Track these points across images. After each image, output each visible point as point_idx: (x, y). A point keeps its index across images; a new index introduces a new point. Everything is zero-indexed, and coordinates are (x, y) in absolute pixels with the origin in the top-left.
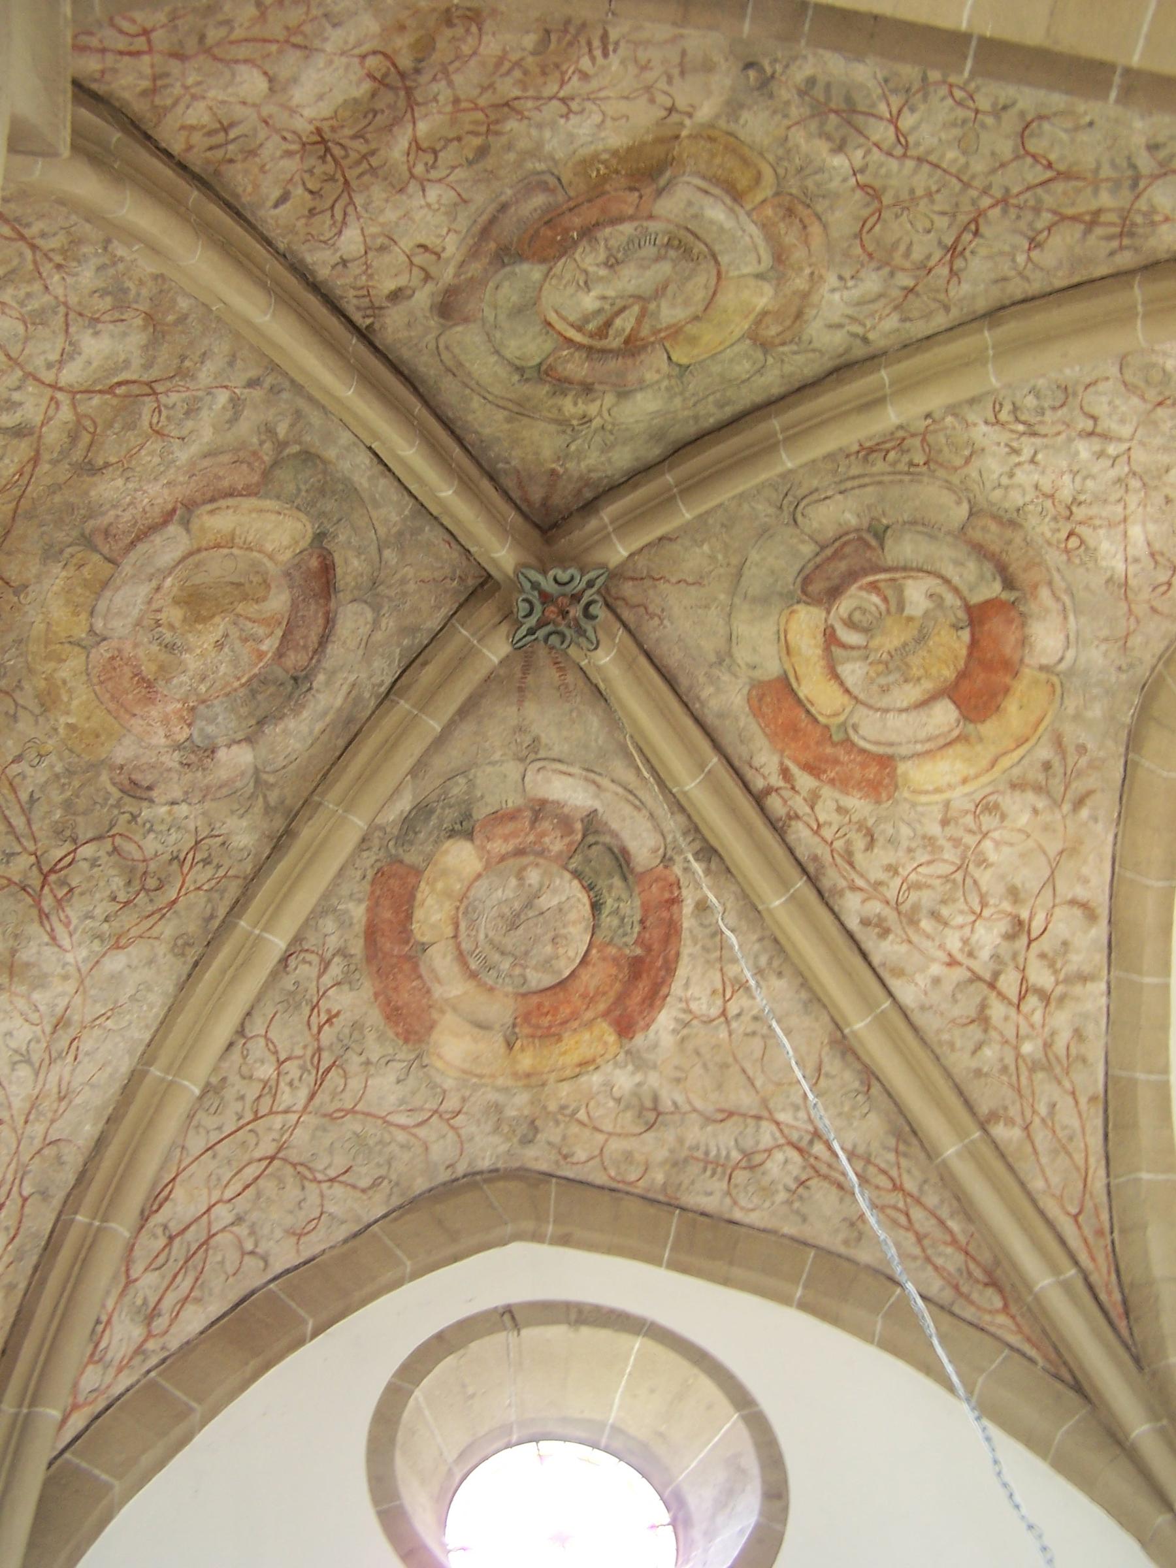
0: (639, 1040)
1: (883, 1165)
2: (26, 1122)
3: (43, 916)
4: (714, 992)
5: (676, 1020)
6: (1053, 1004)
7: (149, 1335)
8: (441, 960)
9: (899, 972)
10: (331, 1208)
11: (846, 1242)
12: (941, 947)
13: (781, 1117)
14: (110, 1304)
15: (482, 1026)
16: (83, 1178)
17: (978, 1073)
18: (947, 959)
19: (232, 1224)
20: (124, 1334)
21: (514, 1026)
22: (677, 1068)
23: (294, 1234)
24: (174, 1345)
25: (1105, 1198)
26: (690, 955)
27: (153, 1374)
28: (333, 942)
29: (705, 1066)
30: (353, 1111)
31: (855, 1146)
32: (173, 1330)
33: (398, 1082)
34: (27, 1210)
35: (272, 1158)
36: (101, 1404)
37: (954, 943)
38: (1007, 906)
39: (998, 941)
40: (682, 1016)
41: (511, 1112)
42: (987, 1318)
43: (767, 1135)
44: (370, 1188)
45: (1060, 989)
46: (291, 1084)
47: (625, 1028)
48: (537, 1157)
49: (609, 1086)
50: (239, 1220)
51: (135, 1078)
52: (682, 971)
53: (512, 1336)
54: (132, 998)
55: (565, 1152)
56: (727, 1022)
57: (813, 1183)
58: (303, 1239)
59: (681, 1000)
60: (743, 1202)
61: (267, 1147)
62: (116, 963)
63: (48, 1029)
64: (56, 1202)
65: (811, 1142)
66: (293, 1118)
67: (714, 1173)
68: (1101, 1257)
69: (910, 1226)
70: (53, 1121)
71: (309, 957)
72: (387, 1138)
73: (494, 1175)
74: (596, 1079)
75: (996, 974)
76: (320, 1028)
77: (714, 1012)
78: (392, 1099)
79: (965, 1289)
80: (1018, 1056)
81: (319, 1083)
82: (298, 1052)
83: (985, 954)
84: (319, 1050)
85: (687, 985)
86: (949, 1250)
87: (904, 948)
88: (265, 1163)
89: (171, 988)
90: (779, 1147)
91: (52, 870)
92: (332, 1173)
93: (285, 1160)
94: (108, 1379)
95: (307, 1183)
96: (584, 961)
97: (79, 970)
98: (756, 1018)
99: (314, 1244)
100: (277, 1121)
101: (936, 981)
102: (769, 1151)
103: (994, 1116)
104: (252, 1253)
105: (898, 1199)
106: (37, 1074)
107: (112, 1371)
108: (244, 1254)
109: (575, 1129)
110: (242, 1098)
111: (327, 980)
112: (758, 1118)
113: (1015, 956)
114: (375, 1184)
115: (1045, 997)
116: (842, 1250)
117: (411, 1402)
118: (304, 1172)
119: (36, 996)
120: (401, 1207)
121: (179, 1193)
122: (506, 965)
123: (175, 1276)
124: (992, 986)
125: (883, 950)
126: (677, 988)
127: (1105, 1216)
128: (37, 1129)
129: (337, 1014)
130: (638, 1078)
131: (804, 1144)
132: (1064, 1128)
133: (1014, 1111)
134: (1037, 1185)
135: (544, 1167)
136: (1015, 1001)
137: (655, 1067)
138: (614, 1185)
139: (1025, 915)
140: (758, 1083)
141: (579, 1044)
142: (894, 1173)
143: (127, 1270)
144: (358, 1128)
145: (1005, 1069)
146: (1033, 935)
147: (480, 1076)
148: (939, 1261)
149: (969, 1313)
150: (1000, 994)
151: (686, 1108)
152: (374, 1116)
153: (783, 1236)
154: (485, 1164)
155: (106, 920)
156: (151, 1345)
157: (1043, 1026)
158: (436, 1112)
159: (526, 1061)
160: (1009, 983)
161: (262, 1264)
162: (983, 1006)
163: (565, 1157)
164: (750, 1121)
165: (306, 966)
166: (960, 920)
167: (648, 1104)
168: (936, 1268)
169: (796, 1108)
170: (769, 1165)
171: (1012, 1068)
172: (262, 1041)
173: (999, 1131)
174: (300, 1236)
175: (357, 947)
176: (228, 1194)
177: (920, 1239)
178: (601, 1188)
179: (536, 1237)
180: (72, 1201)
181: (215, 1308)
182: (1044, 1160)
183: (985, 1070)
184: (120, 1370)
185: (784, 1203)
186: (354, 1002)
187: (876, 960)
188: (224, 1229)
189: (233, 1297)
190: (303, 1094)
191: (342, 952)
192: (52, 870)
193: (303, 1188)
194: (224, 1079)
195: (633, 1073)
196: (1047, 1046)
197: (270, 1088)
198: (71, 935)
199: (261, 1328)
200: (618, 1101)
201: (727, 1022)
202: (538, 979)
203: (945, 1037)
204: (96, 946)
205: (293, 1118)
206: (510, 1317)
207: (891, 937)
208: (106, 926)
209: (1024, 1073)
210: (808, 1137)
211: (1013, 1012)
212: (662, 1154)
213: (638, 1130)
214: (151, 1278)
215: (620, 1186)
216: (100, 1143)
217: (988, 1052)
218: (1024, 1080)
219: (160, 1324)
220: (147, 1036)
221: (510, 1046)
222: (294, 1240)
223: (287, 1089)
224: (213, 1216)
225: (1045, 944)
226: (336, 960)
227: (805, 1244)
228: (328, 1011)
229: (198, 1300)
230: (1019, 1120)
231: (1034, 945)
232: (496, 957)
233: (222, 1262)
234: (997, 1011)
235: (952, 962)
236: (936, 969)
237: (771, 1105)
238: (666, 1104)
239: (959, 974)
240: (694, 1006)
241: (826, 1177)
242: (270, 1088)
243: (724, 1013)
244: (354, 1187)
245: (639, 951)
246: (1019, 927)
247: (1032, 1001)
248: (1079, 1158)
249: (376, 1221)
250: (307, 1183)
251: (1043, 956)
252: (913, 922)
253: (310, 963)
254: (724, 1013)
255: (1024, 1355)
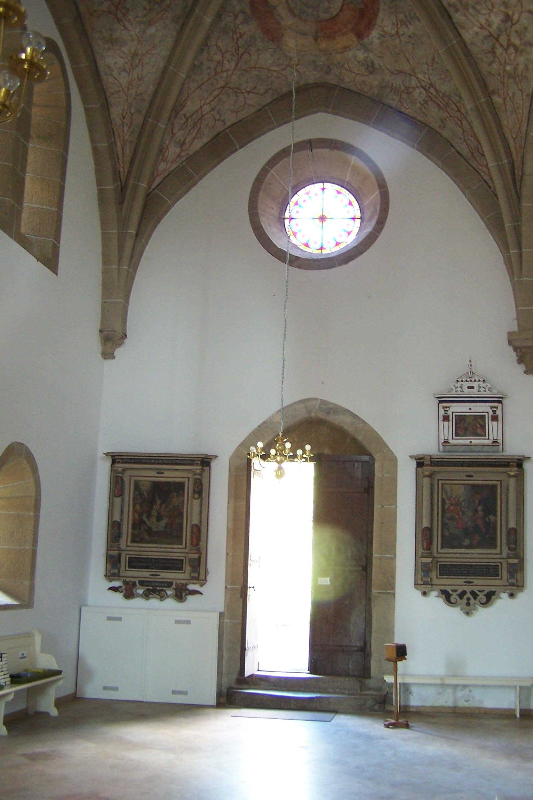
0: (366, 40)
1: (455, 101)
2: (128, 89)
3: (120, 21)
4: (393, 24)
5: (379, 34)
6: (519, 53)
7: (182, 150)
8: (282, 11)
9: (463, 28)
10: (249, 102)
11: (440, 127)
12: (478, 21)
13: (420, 76)
14: (167, 142)
15: (304, 34)
16: (151, 103)
17: (490, 74)
18: (480, 26)
19: (210, 111)
20: (173, 151)
21: (317, 32)
22: (381, 52)
23: (235, 112)
24: (191, 153)
25: (524, 135)
26: (383, 9)
27: (184, 163)
28: (238, 8)
29: (391, 53)
30: (255, 68)
31: (445, 92)
32: (191, 148)
33: (271, 56)
34: (133, 117)
35: (223, 88)
36: (167, 173)
37: (482, 20)
38: (503, 9)
39: (500, 22)
40: (381, 32)
41: (319, 63)
42: (480, 167)
43: (414, 82)
44: (265, 93)
45: (522, 47)
46: (228, 61)
47: (360, 36)
48: (331, 79)
49: (355, 57)
50: (213, 109)
51: (166, 68)
52: (381, 15)
53: (309, 152)
54: (161, 41)
55: (341, 78)
56: (399, 37)
57: (430, 103)
58: (239, 113)
59: (380, 27)
60: (405, 105)
61: (222, 83)
62: (152, 30)
63: (130, 58)
64: (144, 113)
65: (429, 87)
66: (230, 73)
67: (395, 93)
68: (519, 157)
69: (461, 127)
70: (138, 88)
71: (231, 14)
72: (270, 75)
73: (316, 85)
74: (350, 54)
75: (499, 36)
76: (238, 40)
77: (394, 32)
78: (270, 61)
79: (475, 155)
80: (505, 70)
81: (239, 59)
82: (230, 49)
83: (495, 26)
84: (238, 47)
85: (382, 21)
86: (473, 139)
87: (464, 18)
88: (221, 89)
89: (175, 34)
90: (418, 87)
91: (119, 4)
92: (248, 89)
93: (229, 87)
94: (168, 165)
95: (238, 94)
96: (341, 9)
97: (138, 37)
98: (410, 37)
99: (243, 114)
100: (225, 75)
101: (477, 33)
102: (414, 88)
103: (494, 92)
104: (219, 120)
105: (457, 114)
106: (129, 75)
107: (169, 163)
108: (215, 120)
109: (344, 71)
110: (210, 68)
111: (238, 22)
112: (410, 75)
113: (506, 29)
114: (267, 91)
115: (516, 48)
116: (438, 129)
117: (269, 174)
118: (237, 91)
119: (123, 49)
120: (277, 99)
121: (189, 103)
122: (310, 11)
123: (190, 131)
124: (497, 40)
125: (458, 17)
126: (379, 22)
127: (523, 142)
128: (133, 91)
129: (244, 34)
130: (366, 55)
131: (427, 88)
132: (517, 103)
133: (501, 92)
134: (504, 122)
135: (334, 82)
136: (505, 47)
137: (371, 52)
138: (359, 91)
139: (510, 13)
140: (411, 62)
141: (342, 41)
142: (458, 105)
143: (172, 131)
144: (257, 73)
145: (499, 75)
146: (514, 22)
147: (305, 51)
148: (469, 142)
149: (474, 164)
150: (500, 43)
151: (384, 68)
152: (263, 68)
153: (418, 120)
154: (311, 81)
155: (144, 16)
156: (182, 154)
157: (514, 61)
158: (288, 65)
159: (323, 45)
160: (503, 40)
161: (223, 123)
162: (494, 47)
163: (342, 80)
164: (407, 76)
165: (229, 18)
166: (484, 11)
167: (370, 64)
168: (467, 145)
169: (425, 73)
170: (414, 93)
171: (502, 75)
172: (215, 47)
173: (495, 98)
174: (237, 113)
175: (248, 10)
176: (208, 101)
177: (464, 132)
178: (355, 92)
179: (326, 111)
180: (148, 113)
181: (206, 140)
182: (508, 114)
183: (493, 73)
184: (172, 162)
185: (418, 108)
186: (250, 29)
187: (455, 21)
188: (207, 113)
189: (212, 135)
190: (233, 65)
191: (242, 11)
192: (119, 4)
193: (237, 96)
194: (202, 63)
195: (364, 53)
196: (515, 69)
197: (220, 63)
198: (132, 25)
199: (220, 147)
200: (359, 62)
201: (399, 37)
202: (324, 16)
203: (480, 56)
204: (142, 26)
205: (230, 73)
206: (310, 144)
207: (459, 13)
208: (145, 19)
209: (506, 78)
210: (428, 85)
211: (504, 52)
212: (376, 83)
213: (367, 74)
214: (181, 133)
215: (362, 93)
216: (156, 92)
217: (495, 66)
218: (506, 81)
219: (185, 147)
220: (169, 53)
221: (316, 40)
222: (235, 114)
223: (227, 63)
224: (203, 109)
225: (518, 27)
226: (240, 14)
227: (425, 125)
228: (240, 33)
229: (200, 138)
230: (502, 96)
231: (513, 26)
232: (305, 8)
233: (208, 124)
234: (499, 50)
235: (482, 27)
236: (476, 29)
237: (416, 71)
238: (377, 66)
239: (485, 33)
240: (386, 29)
241: (434, 101)
242: (220, 63)
243: (397, 33)
244: (257, 94)
245: (363, 6)
246: (508, 18)
247: (512, 50)
248: (520, 116)
249: (267, 105)
250: (238, 94)
251: (516, 32)
252: (467, 9)
253: (230, 16)
254: (397, 33)
255: (488, 184)
